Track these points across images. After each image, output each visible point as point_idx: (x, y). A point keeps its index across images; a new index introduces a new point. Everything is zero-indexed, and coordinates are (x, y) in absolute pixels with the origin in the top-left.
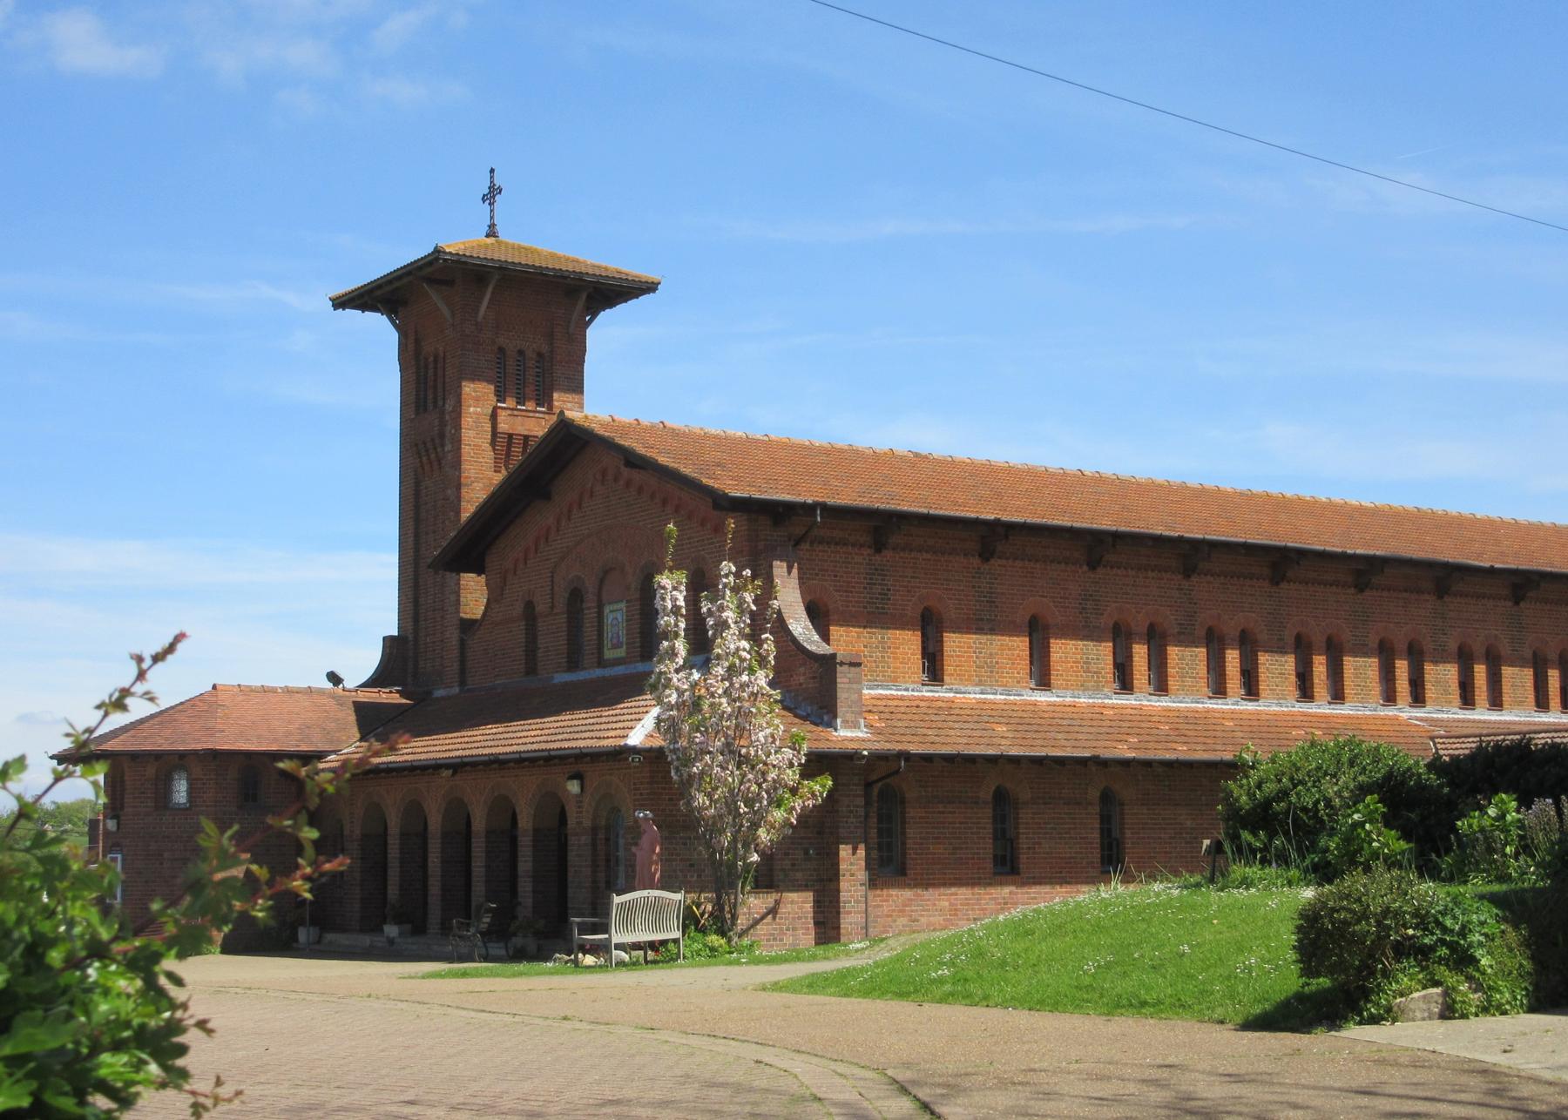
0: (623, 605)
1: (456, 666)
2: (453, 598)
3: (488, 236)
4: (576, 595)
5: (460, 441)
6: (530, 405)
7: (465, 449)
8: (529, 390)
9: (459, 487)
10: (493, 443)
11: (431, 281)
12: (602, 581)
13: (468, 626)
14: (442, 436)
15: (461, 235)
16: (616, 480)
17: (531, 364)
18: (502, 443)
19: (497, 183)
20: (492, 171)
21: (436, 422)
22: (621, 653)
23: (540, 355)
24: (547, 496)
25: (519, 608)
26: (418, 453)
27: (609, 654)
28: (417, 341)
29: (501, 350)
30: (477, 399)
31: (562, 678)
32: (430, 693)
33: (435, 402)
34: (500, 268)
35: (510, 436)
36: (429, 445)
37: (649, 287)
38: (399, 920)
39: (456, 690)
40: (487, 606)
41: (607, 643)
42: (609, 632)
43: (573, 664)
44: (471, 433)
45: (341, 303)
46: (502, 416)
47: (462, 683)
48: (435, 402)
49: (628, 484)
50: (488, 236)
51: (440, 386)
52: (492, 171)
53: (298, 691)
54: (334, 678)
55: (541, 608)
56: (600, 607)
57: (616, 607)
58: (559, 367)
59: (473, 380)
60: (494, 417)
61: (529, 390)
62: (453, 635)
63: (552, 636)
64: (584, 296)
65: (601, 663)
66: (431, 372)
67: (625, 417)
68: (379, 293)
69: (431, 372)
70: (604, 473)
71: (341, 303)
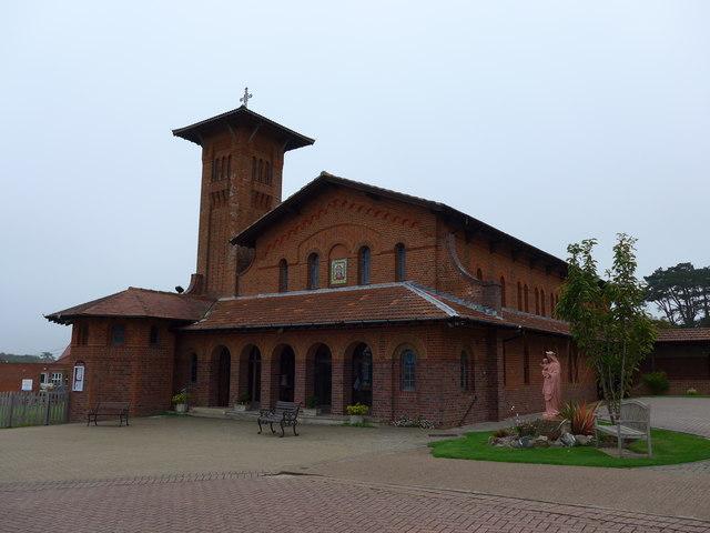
4: (314, 257)
14: (228, 190)
22: (341, 281)
27: (333, 282)
33: (222, 176)
38: (241, 401)
42: (334, 273)
48: (222, 176)
65: (330, 286)
71: (178, 133)
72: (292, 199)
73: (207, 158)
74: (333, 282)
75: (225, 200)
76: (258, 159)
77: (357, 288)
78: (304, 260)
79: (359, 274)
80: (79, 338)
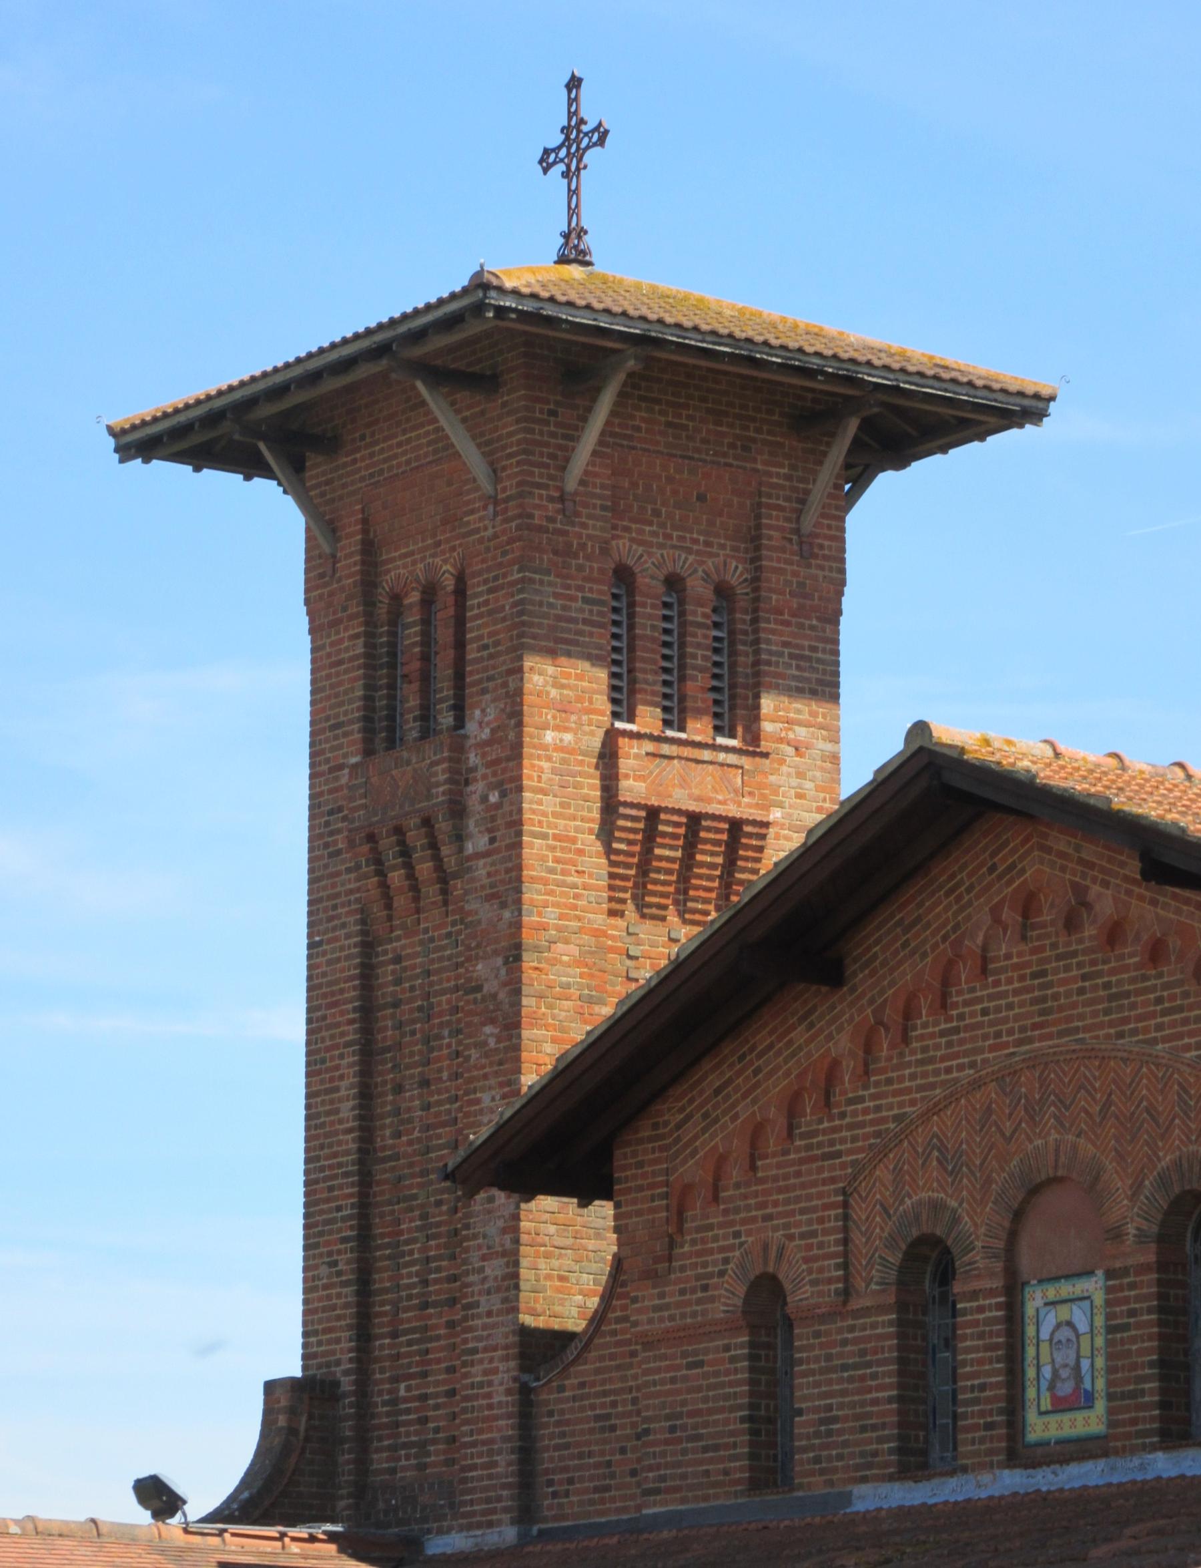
0: (1094, 1286)
1: (505, 1464)
2: (495, 1269)
3: (563, 260)
4: (929, 1264)
5: (516, 824)
6: (699, 729)
7: (534, 850)
8: (697, 685)
9: (514, 955)
10: (607, 833)
11: (440, 375)
12: (1018, 1216)
13: (543, 1350)
14: (458, 810)
15: (525, 263)
16: (1071, 924)
17: (699, 614)
18: (647, 847)
19: (591, 114)
20: (574, 83)
21: (441, 774)
22: (1090, 1422)
23: (723, 591)
24: (832, 974)
25: (728, 1296)
26: (378, 861)
27: (1041, 1427)
28: (369, 549)
29: (623, 575)
30: (564, 709)
31: (878, 1497)
32: (414, 1544)
33: (426, 715)
34: (643, 340)
35: (653, 814)
36: (416, 838)
37: (1022, 409)
39: (508, 1534)
40: (609, 1296)
41: (1035, 1395)
42: (1042, 1364)
43: (913, 1462)
44: (549, 804)
45: (143, 442)
46: (632, 756)
47: (525, 1514)
48: (426, 715)
49: (1114, 934)
50: (563, 260)
51: (444, 689)
52: (574, 83)
53: (64, 1532)
54: (158, 1496)
55: (803, 1294)
56: (1013, 1289)
57: (1066, 1289)
58: (749, 637)
59: (552, 653)
60: (608, 757)
61: (697, 685)
62: (496, 1378)
63: (845, 1375)
64: (852, 426)
65: (1018, 1453)
66: (411, 636)
67: (1144, 757)
68: (267, 410)
69: (411, 636)
70: (1028, 905)
71: (143, 442)
72: (568, 1073)
73: (324, 528)
74: (1041, 1427)
75: (443, 879)
76: (698, 587)
77: (1163, 1465)
78: (875, 1282)
79: (1174, 1368)
80: (648, 814)
